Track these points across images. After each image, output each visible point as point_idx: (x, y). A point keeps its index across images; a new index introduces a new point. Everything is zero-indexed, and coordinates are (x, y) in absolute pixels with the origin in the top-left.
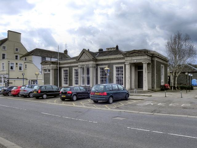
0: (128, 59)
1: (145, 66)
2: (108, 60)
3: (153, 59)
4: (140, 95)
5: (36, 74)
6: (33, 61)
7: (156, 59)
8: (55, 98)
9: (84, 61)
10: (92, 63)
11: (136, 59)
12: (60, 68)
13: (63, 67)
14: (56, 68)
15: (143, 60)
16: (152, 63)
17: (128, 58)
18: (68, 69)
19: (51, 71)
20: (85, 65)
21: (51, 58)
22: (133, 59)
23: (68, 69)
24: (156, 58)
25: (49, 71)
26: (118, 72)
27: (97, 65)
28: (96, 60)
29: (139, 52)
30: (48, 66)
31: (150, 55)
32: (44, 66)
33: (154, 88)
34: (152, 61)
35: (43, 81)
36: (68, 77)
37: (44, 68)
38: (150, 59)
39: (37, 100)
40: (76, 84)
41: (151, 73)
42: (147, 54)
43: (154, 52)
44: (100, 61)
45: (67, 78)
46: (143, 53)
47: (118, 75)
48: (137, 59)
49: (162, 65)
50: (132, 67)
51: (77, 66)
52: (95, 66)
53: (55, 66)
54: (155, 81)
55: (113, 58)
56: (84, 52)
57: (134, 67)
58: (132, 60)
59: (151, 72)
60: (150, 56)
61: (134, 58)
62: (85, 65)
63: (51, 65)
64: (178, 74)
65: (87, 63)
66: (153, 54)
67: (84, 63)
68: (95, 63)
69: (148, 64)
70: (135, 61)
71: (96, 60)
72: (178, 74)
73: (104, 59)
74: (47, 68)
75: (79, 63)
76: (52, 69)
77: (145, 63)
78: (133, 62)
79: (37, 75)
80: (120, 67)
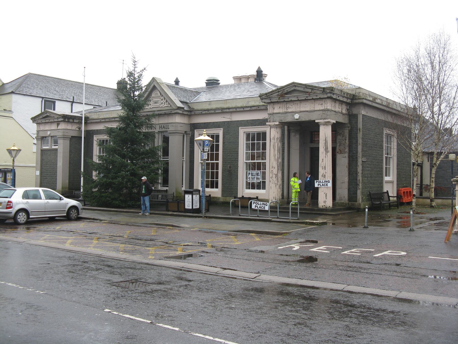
0: (277, 109)
1: (325, 133)
3: (355, 111)
5: (10, 151)
6: (13, 110)
7: (363, 112)
8: (68, 222)
11: (298, 112)
12: (89, 135)
13: (98, 132)
14: (75, 134)
15: (326, 116)
19: (60, 141)
20: (158, 127)
21: (73, 102)
22: (290, 110)
23: (220, 132)
24: (362, 107)
25: (56, 143)
26: (253, 149)
27: (194, 127)
30: (54, 127)
31: (341, 99)
32: (42, 127)
33: (356, 201)
34: (352, 117)
35: (38, 173)
37: (42, 134)
38: (344, 112)
40: (212, 187)
41: (347, 155)
42: (329, 95)
43: (358, 91)
44: (201, 114)
46: (318, 92)
47: (253, 158)
49: (386, 131)
50: (292, 134)
52: (187, 129)
53: (75, 127)
54: (360, 177)
56: (154, 88)
57: (298, 136)
58: (286, 113)
59: (347, 150)
60: (342, 102)
61: (292, 108)
63: (63, 126)
64: (438, 159)
66: (354, 95)
69: (336, 128)
70: (297, 116)
71: (191, 111)
72: (438, 159)
73: (211, 110)
74: (49, 133)
76: (64, 137)
77: (326, 124)
78: (289, 119)
79: (14, 153)
80: (259, 134)
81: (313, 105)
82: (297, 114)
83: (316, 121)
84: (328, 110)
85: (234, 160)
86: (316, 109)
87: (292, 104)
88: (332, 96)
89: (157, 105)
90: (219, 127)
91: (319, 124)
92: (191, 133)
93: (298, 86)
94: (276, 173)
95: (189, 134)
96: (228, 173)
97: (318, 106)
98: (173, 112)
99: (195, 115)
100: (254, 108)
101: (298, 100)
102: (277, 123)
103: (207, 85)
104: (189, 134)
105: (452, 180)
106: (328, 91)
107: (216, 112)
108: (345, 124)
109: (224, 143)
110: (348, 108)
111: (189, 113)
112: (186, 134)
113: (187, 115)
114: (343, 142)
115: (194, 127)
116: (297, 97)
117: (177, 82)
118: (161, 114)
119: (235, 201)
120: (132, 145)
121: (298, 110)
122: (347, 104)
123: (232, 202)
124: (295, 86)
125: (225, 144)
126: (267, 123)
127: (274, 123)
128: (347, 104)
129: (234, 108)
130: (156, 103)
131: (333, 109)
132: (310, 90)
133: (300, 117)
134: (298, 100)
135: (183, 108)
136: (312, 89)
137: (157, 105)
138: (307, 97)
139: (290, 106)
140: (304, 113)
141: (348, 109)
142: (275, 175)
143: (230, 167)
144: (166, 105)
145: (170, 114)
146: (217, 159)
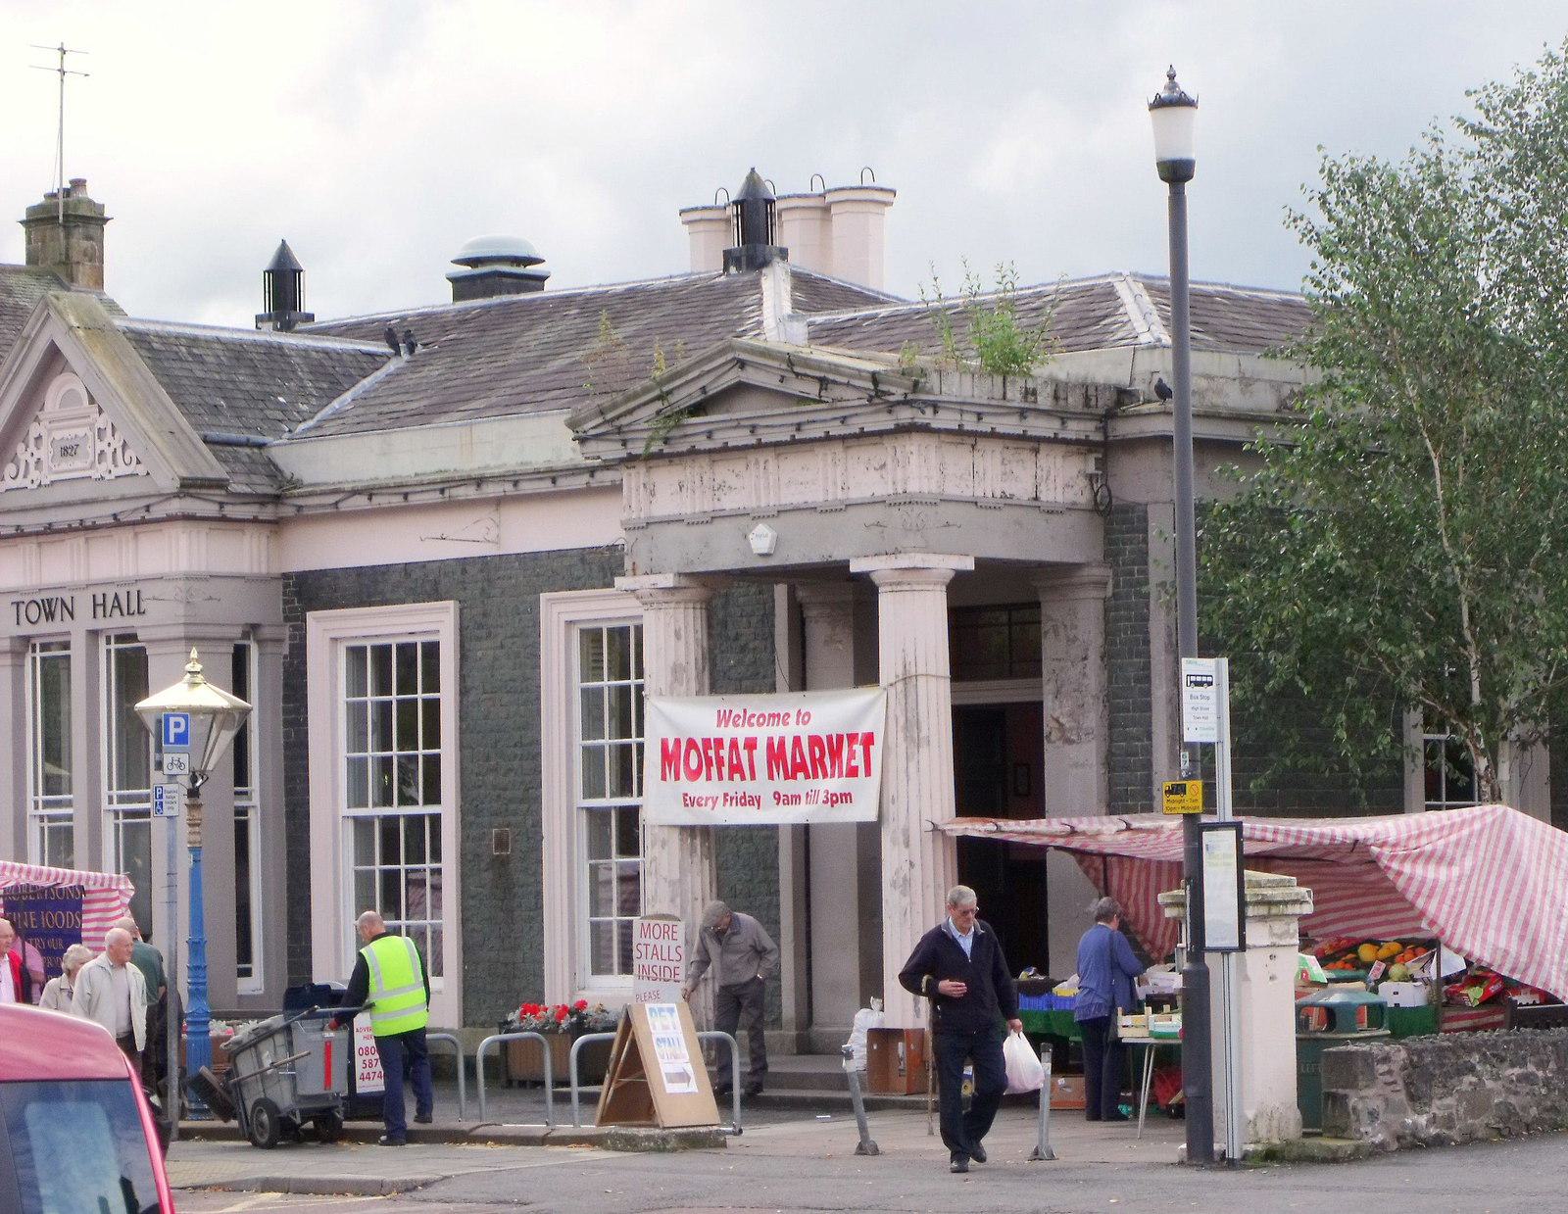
0: (669, 493)
2: (448, 493)
4: (510, 1127)
9: (60, 517)
10: (173, 554)
16: (1111, 555)
17: (666, 478)
18: (436, 622)
20: (83, 606)
22: (729, 502)
28: (278, 504)
29: (796, 387)
36: (448, 808)
39: (1100, 1128)
42: (905, 415)
44: (336, 514)
45: (420, 838)
48: (791, 497)
50: (818, 631)
51: (599, 567)
52: (268, 609)
55: (538, 474)
58: (715, 517)
61: (746, 486)
62: (83, 606)
65: (110, 561)
67: (59, 567)
68: (243, 554)
70: (761, 539)
75: (632, 479)
81: (840, 469)
82: (761, 528)
83: (854, 568)
84: (909, 501)
85: (519, 794)
86: (855, 495)
87: (739, 466)
88: (926, 417)
89: (75, 467)
90: (435, 594)
91: (874, 577)
92: (287, 632)
93: (757, 366)
94: (676, 875)
95: (280, 641)
96: (487, 876)
97: (862, 476)
98: (158, 512)
99: (302, 517)
100: (491, 490)
101: (760, 446)
102: (668, 580)
103: (457, 297)
104: (280, 641)
105: (1162, 898)
106: (898, 394)
107: (414, 499)
108: (1076, 567)
109: (463, 691)
110: (1091, 468)
111: (268, 513)
112: (260, 642)
113: (255, 521)
114: (1073, 673)
115: (309, 592)
116: (753, 429)
117: (283, 282)
118: (95, 527)
119: (504, 1044)
120: (1303, 454)
121: (769, 500)
122: (1084, 446)
123: (487, 1060)
124: (742, 364)
125: (472, 697)
126: (618, 581)
127: (653, 578)
128: (1084, 446)
129: (501, 478)
130: (67, 451)
131: (952, 490)
132: (812, 389)
133: (778, 542)
134: (760, 446)
135: (220, 484)
136: (824, 382)
137: (75, 467)
138: (799, 427)
139: (731, 480)
140: (804, 517)
141: (1091, 478)
142: (672, 883)
143: (501, 843)
144: (122, 470)
145: (144, 522)
146: (433, 796)
